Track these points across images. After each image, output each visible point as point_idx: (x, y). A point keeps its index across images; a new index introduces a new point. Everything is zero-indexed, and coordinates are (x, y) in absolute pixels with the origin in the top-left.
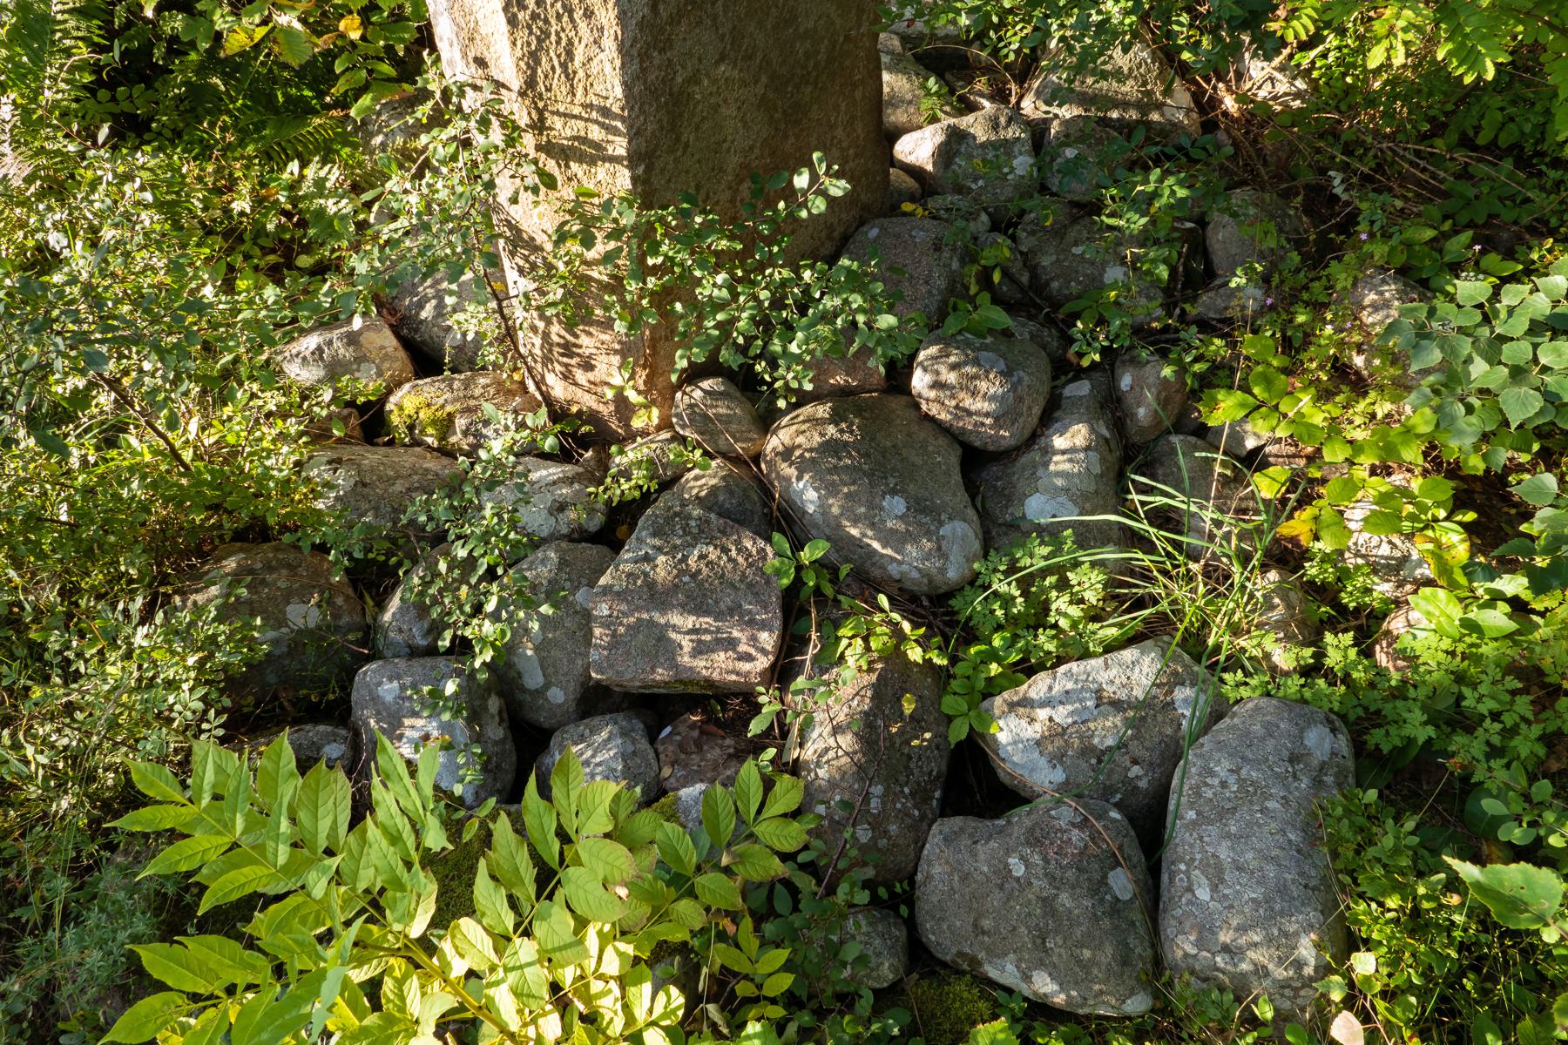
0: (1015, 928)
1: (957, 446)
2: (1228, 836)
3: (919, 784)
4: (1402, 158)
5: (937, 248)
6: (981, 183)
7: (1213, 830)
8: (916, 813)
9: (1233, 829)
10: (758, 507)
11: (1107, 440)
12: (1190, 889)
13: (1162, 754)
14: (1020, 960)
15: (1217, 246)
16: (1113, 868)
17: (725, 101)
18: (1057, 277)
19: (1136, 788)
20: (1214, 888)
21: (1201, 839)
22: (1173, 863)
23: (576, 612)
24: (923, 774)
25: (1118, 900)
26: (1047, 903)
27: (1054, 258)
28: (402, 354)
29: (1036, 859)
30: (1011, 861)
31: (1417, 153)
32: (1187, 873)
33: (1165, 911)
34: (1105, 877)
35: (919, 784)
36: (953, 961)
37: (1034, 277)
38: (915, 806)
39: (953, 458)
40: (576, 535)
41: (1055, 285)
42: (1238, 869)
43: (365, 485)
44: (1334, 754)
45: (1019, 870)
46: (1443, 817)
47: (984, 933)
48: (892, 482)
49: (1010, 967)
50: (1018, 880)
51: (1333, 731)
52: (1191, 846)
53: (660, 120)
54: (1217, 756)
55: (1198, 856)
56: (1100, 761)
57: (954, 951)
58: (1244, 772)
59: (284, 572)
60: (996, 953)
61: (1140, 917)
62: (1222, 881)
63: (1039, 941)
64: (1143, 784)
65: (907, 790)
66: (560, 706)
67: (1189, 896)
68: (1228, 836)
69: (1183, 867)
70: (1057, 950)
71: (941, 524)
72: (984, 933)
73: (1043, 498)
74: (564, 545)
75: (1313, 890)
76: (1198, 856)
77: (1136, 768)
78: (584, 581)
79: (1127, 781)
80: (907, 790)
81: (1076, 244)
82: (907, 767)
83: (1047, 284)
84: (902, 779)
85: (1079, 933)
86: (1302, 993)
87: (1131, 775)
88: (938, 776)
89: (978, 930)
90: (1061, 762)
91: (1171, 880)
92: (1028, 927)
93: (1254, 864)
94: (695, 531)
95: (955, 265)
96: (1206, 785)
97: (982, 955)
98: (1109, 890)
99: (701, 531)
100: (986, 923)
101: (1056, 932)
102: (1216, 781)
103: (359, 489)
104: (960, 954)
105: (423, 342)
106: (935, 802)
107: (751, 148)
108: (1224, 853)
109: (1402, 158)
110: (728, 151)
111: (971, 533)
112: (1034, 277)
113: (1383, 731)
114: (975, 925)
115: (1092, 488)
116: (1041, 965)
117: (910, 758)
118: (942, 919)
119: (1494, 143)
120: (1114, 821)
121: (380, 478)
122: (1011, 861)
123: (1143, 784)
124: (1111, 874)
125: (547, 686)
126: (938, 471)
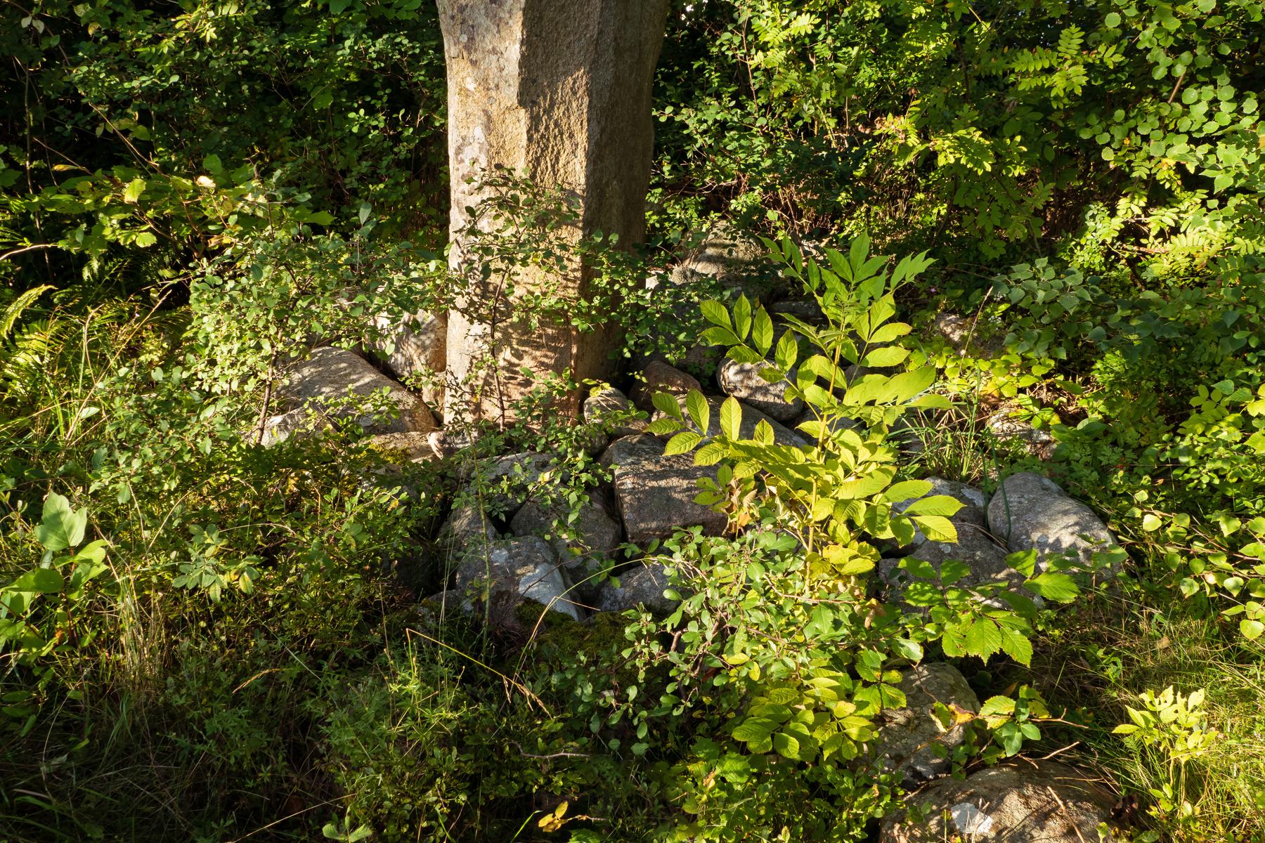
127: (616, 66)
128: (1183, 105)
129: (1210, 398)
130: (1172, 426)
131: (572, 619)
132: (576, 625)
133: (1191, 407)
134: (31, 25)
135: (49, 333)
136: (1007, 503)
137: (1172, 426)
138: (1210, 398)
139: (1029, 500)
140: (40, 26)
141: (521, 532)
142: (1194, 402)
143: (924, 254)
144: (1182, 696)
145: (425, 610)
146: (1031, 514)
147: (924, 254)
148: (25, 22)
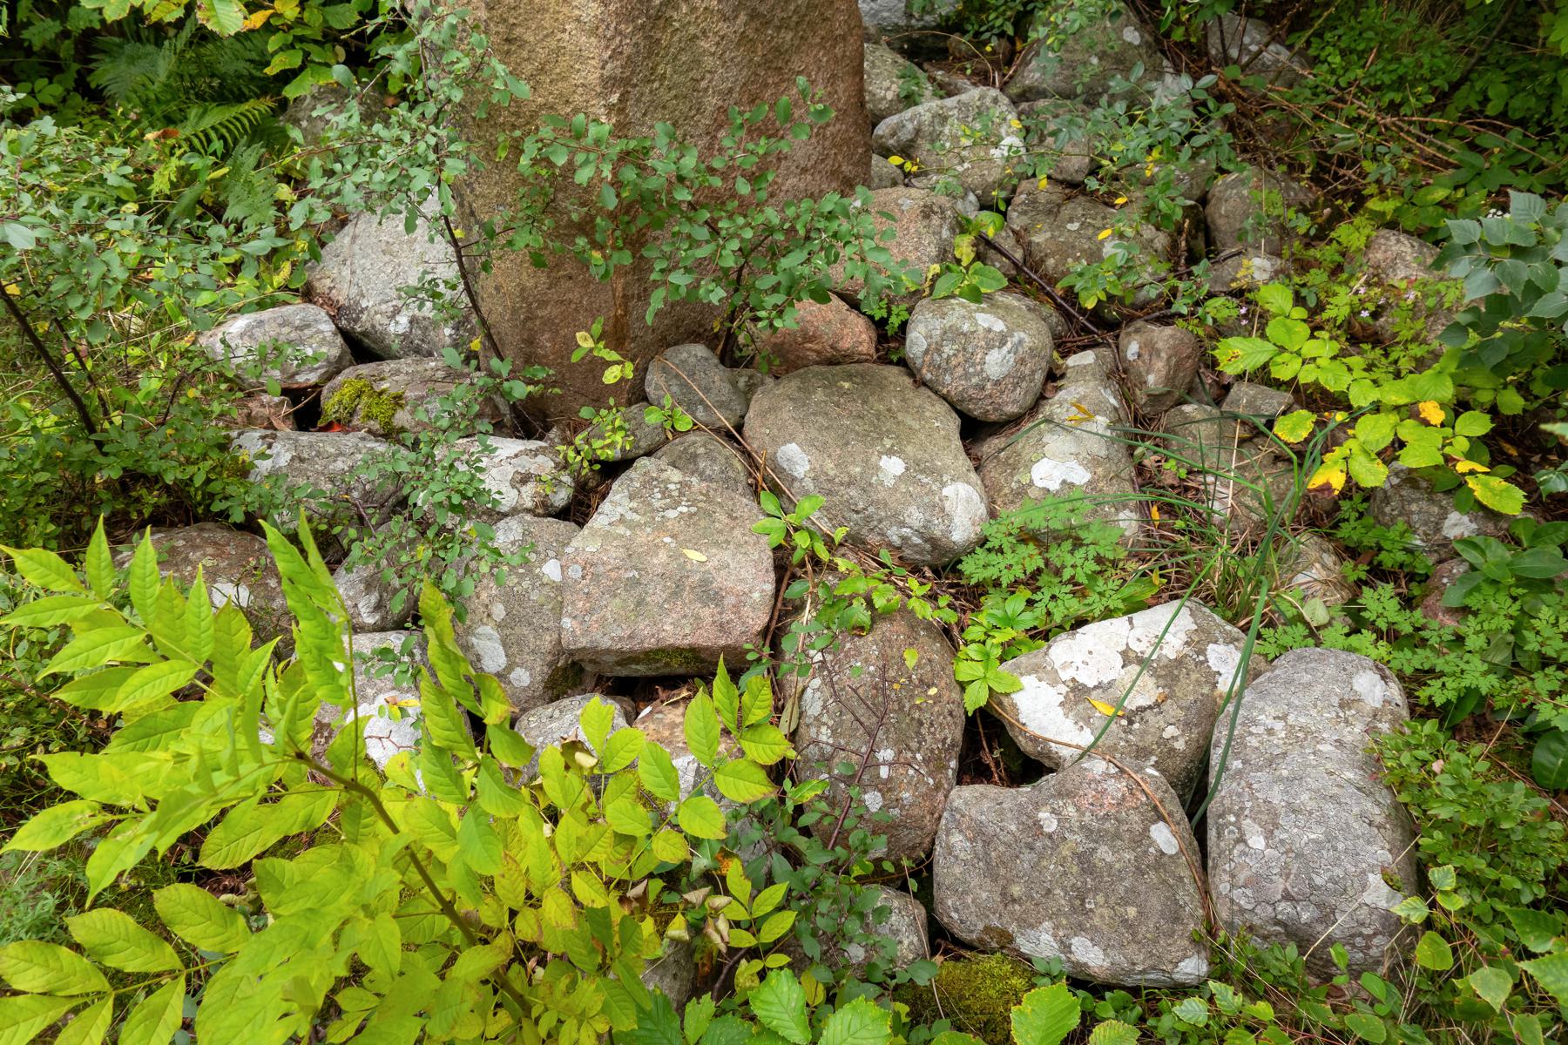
0: (1049, 891)
1: (954, 415)
2: (1280, 779)
3: (932, 751)
4: (1408, 132)
5: (926, 216)
6: (966, 165)
7: (1263, 776)
8: (931, 781)
9: (1285, 773)
10: (742, 477)
11: (1116, 409)
12: (1242, 840)
13: (1198, 713)
14: (1056, 927)
15: (1220, 222)
16: (1155, 822)
17: (704, 32)
18: (1053, 254)
19: (1173, 749)
20: (1269, 835)
21: (1250, 786)
22: (1221, 816)
23: (543, 585)
24: (936, 741)
25: (1163, 854)
26: (1084, 860)
27: (1048, 235)
28: (339, 340)
29: (1071, 811)
30: (1041, 815)
31: (1422, 126)
32: (1238, 825)
33: (1215, 868)
34: (1146, 829)
35: (932, 751)
36: (981, 940)
37: (1028, 254)
38: (930, 774)
39: (953, 424)
40: (540, 511)
41: (1051, 262)
42: (1294, 811)
43: (302, 460)
44: (1387, 702)
45: (1051, 825)
46: (1510, 774)
47: (1014, 901)
48: (888, 443)
49: (1046, 938)
50: (1050, 836)
51: (1384, 678)
52: (1239, 795)
53: (636, 44)
54: (1260, 704)
55: (1248, 805)
56: (1131, 722)
57: (981, 926)
58: (1291, 719)
59: (210, 550)
60: (1026, 924)
61: (1188, 873)
62: (1276, 826)
63: (1078, 902)
64: (1180, 745)
65: (919, 757)
66: (524, 690)
67: (1240, 847)
68: (1280, 779)
69: (1233, 819)
70: (1098, 911)
71: (943, 485)
72: (1014, 901)
73: (1052, 463)
74: (528, 517)
75: (1378, 827)
76: (1248, 805)
77: (1171, 728)
78: (552, 554)
79: (1163, 742)
80: (919, 757)
81: (1071, 221)
82: (918, 733)
83: (1042, 261)
84: (914, 745)
85: (1121, 890)
86: (1375, 941)
87: (1166, 735)
88: (953, 745)
89: (1008, 900)
90: (1088, 723)
91: (1219, 835)
92: (1064, 888)
93: (1311, 805)
94: (676, 494)
95: (945, 233)
96: (1251, 734)
97: (1012, 928)
98: (1153, 843)
99: (681, 494)
100: (1016, 890)
101: (1096, 890)
102: (1261, 730)
103: (297, 464)
104: (987, 929)
105: (365, 334)
106: (950, 772)
107: (730, 91)
108: (1277, 797)
109: (1408, 132)
110: (706, 90)
111: (976, 497)
112: (1028, 254)
113: (1438, 683)
114: (1003, 895)
115: (1103, 453)
116: (1080, 928)
117: (921, 723)
118: (965, 892)
119: (1503, 115)
120: (1151, 776)
121: (319, 454)
122: (1041, 815)
123: (1180, 745)
124: (1153, 828)
125: (510, 667)
126: (936, 436)
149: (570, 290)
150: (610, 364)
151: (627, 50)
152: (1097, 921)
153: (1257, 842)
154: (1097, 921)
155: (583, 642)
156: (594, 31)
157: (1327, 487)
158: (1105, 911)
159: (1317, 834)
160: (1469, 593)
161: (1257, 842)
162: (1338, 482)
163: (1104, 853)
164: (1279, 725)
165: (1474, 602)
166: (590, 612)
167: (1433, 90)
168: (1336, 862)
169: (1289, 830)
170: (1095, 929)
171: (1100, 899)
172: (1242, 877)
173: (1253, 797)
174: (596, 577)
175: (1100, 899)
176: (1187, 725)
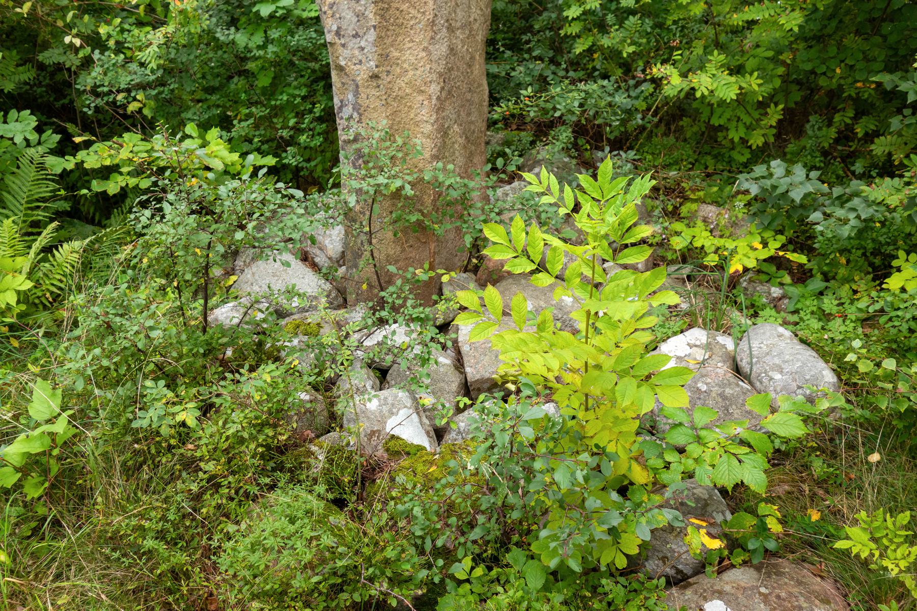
12: (771, 379)
20: (781, 372)
101: (731, 405)
108: (777, 361)
127: (450, 40)
128: (882, 36)
129: (907, 260)
130: (878, 282)
131: (423, 448)
132: (427, 454)
133: (892, 267)
134: (71, 42)
135: (559, 145)
136: (750, 348)
137: (878, 282)
138: (907, 260)
139: (767, 345)
140: (77, 42)
141: (393, 382)
142: (895, 263)
143: (649, 176)
144: (891, 516)
145: (317, 448)
146: (768, 357)
147: (649, 176)
148: (67, 39)
149: (411, 252)
150: (443, 274)
151: (439, 144)
152: (736, 416)
153: (777, 376)
154: (736, 416)
155: (478, 377)
156: (428, 137)
157: (737, 271)
158: (738, 411)
159: (799, 364)
160: (796, 304)
161: (777, 376)
162: (740, 269)
163: (728, 391)
164: (762, 345)
165: (799, 306)
166: (477, 363)
167: (691, 163)
168: (810, 370)
169: (787, 368)
170: (736, 419)
171: (734, 407)
172: (778, 389)
173: (768, 365)
174: (476, 348)
175: (734, 407)
176: (724, 362)
